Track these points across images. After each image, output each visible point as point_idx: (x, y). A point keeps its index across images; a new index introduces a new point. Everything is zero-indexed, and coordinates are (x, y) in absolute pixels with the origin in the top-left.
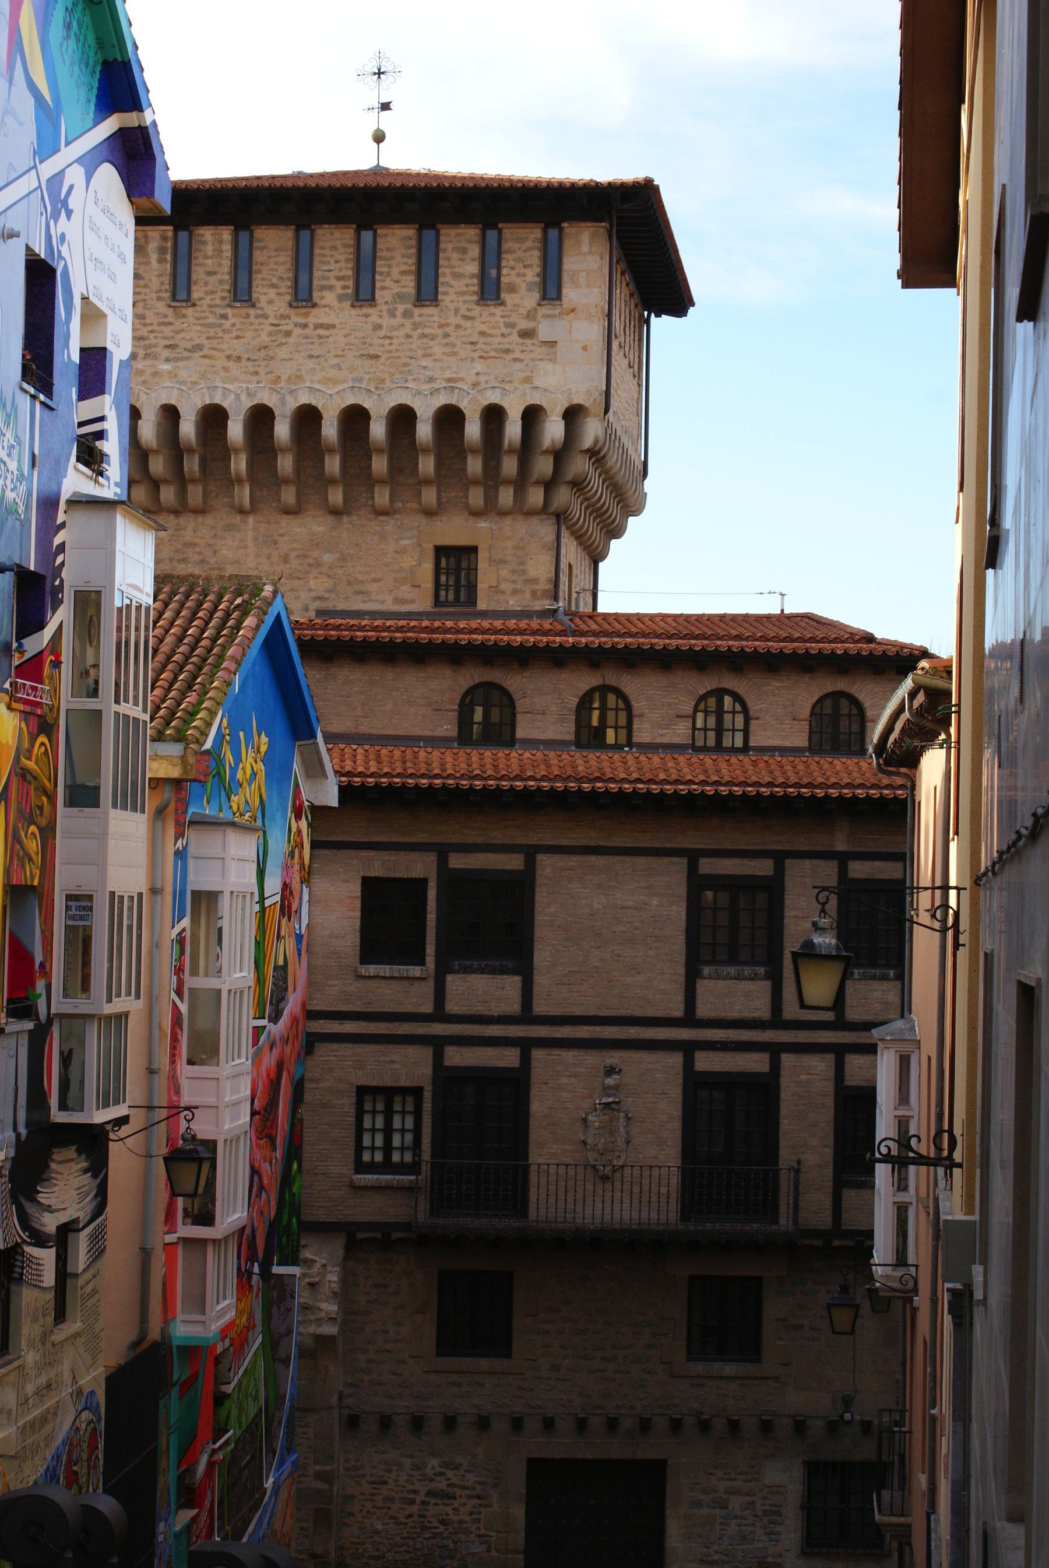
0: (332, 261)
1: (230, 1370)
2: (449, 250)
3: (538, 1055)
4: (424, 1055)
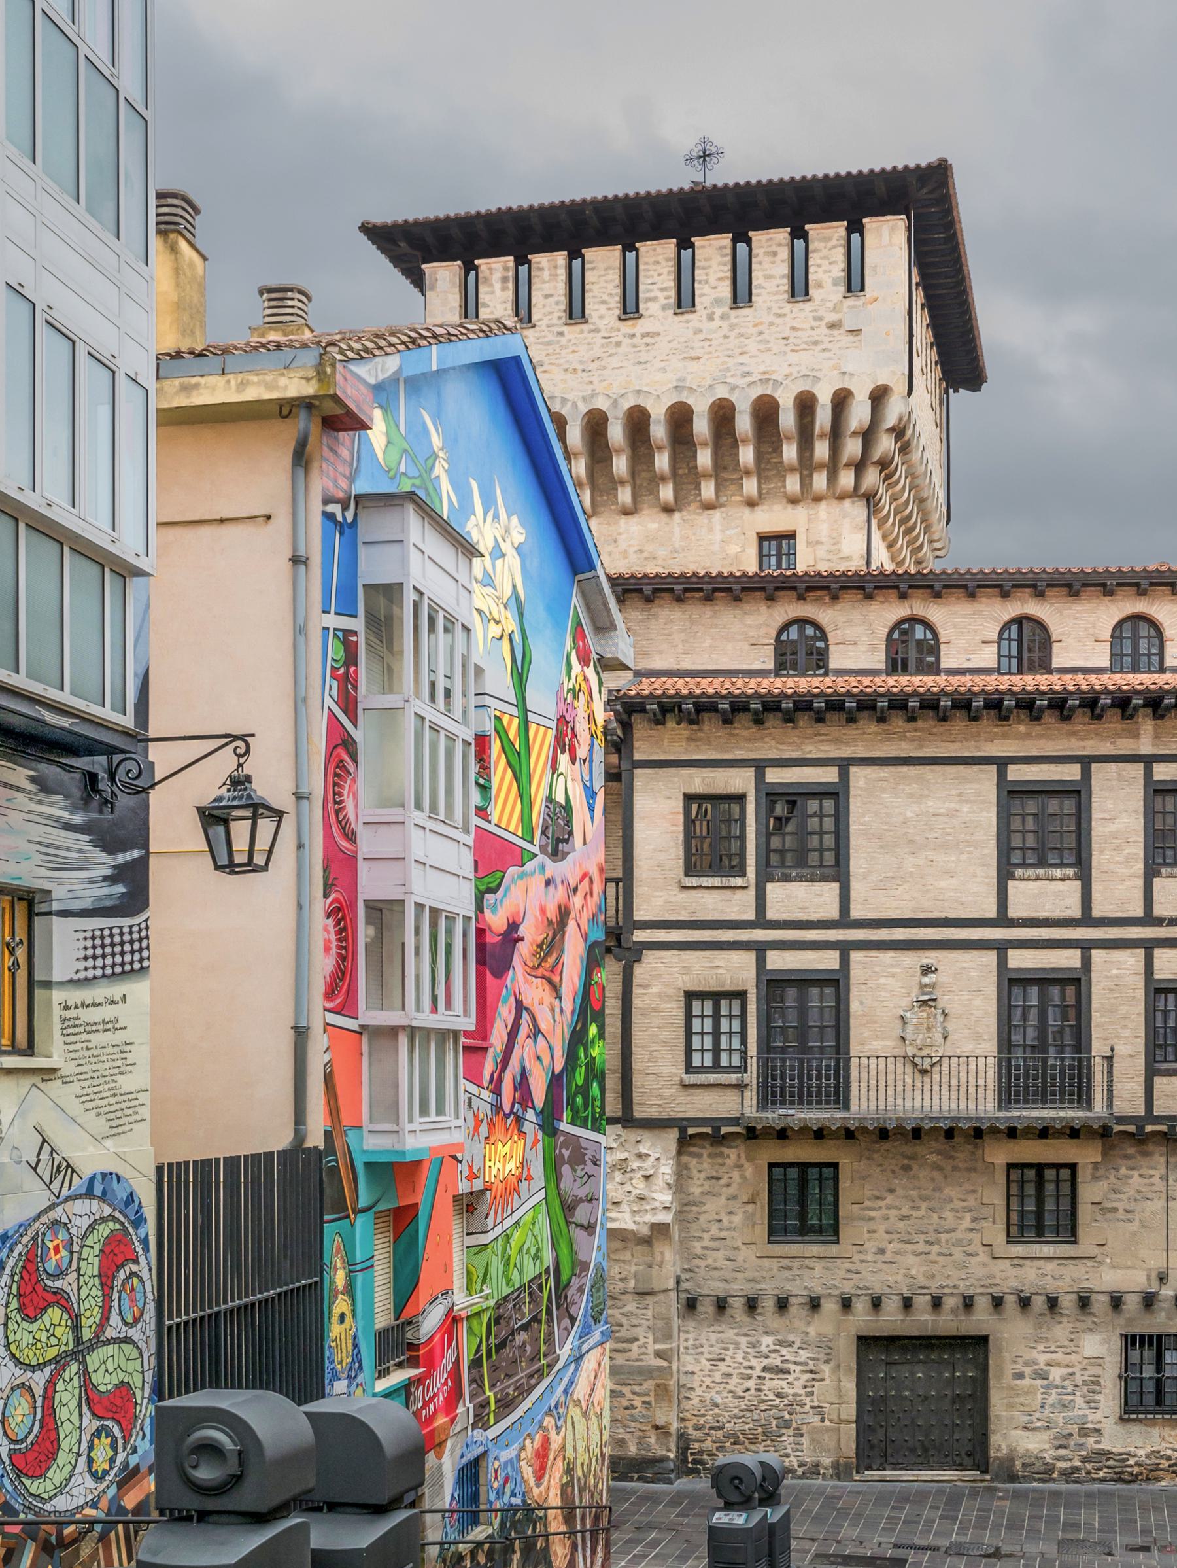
0: (655, 274)
1: (486, 1218)
2: (761, 255)
3: (856, 956)
4: (748, 959)
